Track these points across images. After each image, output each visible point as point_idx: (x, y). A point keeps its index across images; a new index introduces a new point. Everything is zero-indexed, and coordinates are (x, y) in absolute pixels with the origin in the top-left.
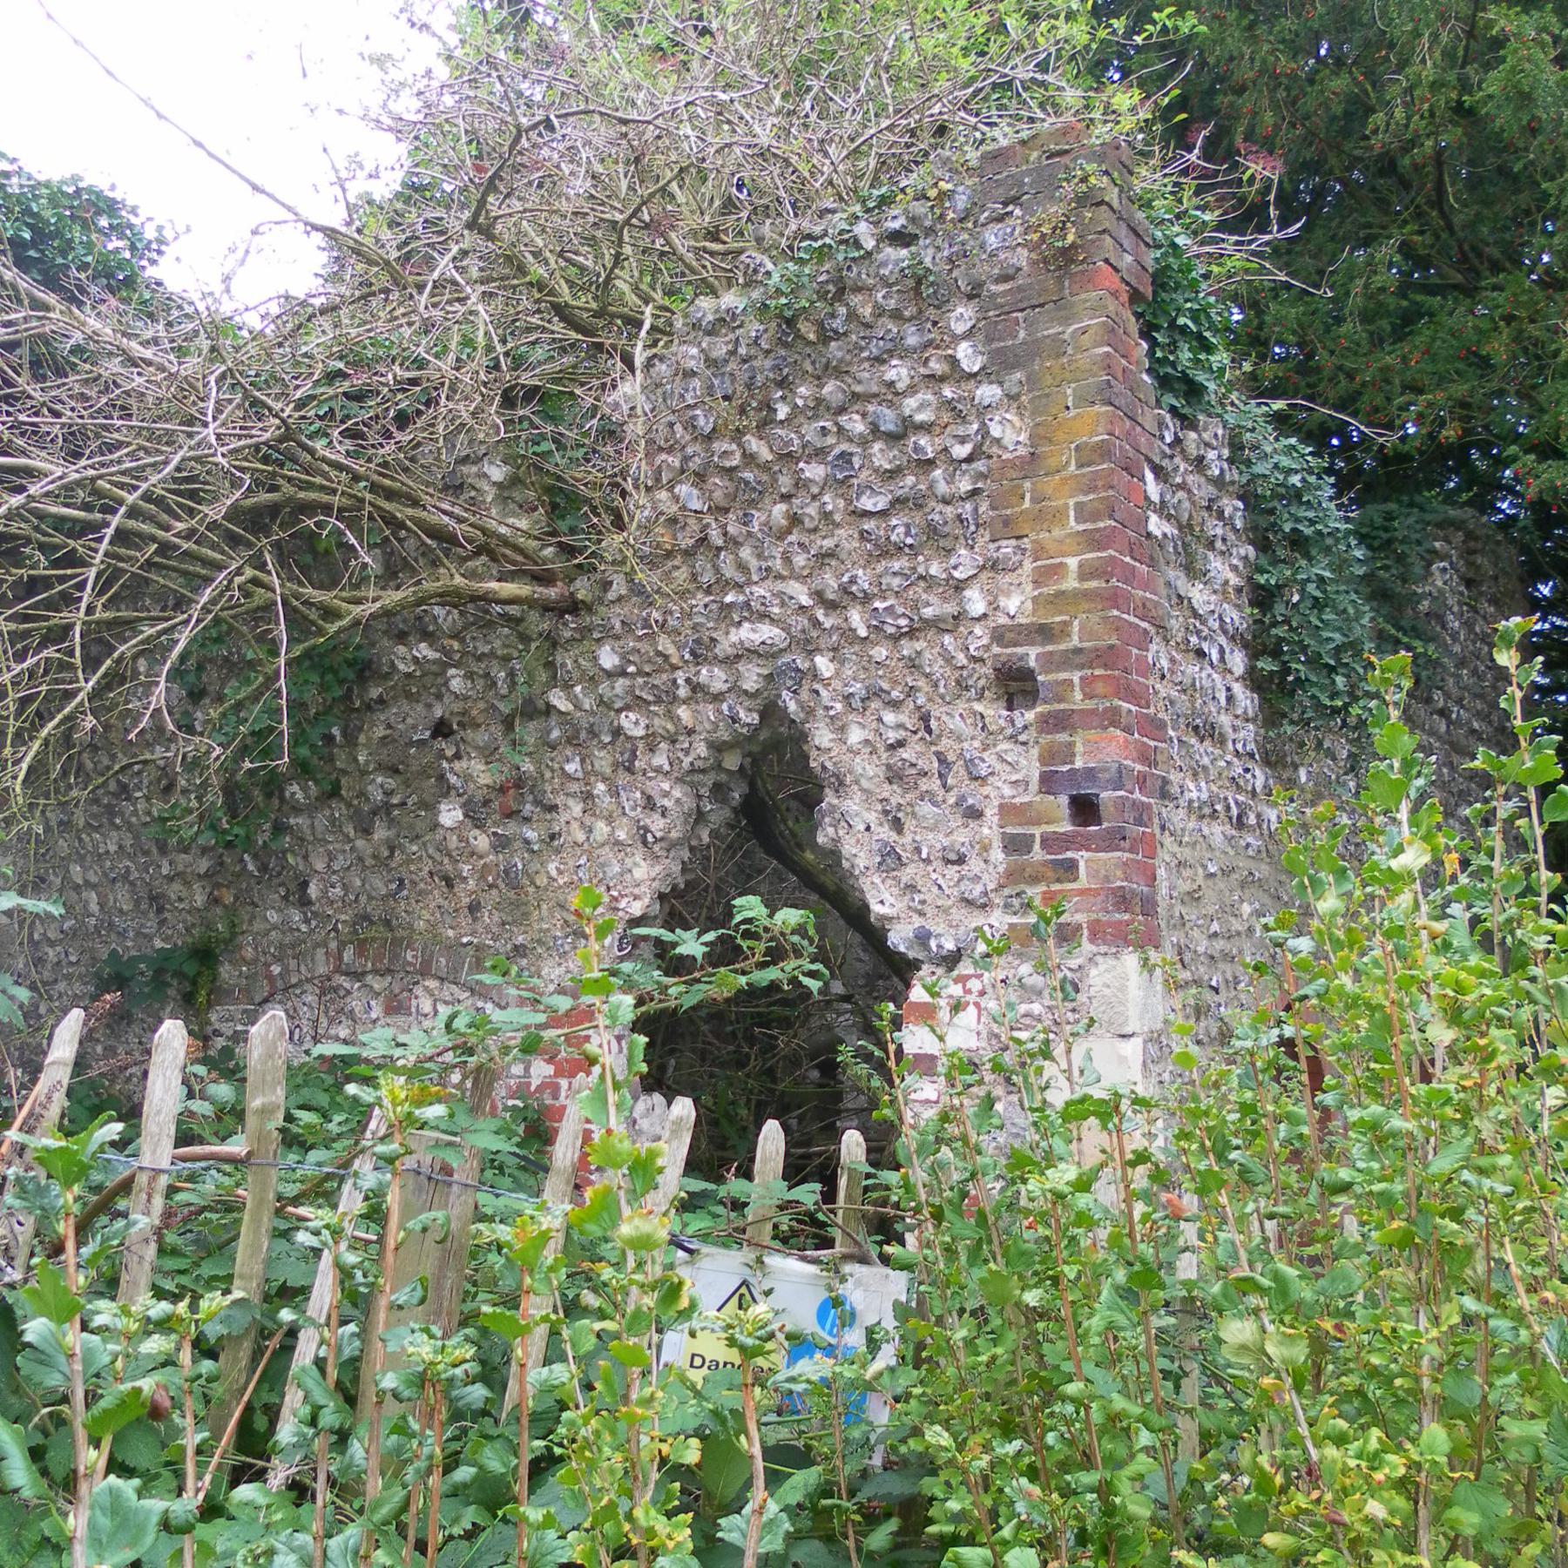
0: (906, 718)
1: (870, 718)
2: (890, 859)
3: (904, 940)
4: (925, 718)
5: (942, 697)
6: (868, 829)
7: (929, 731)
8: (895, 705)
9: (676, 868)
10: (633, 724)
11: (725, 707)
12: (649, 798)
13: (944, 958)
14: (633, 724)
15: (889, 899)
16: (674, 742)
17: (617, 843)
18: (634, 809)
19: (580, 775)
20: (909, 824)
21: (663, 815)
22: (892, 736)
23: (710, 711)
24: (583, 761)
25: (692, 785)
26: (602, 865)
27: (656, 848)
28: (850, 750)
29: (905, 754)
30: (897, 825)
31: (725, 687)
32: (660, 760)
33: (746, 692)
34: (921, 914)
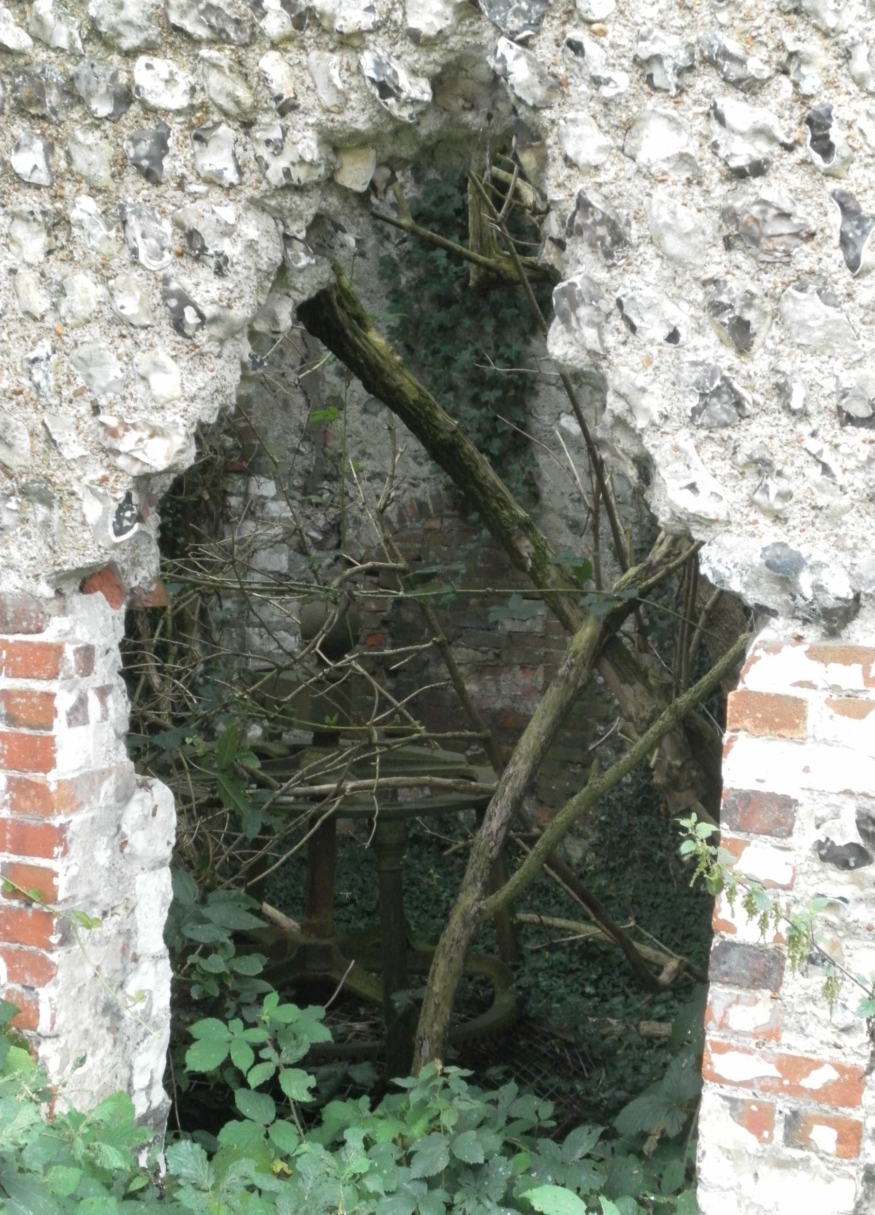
0: (774, 112)
1: (691, 111)
2: (719, 403)
3: (743, 569)
4: (818, 125)
5: (860, 81)
6: (673, 337)
7: (826, 149)
8: (749, 87)
9: (233, 377)
10: (162, 81)
11: (367, 60)
12: (192, 235)
13: (827, 614)
14: (162, 81)
15: (706, 484)
16: (247, 125)
17: (118, 320)
18: (158, 254)
19: (42, 177)
20: (765, 334)
21: (219, 272)
22: (743, 153)
23: (330, 66)
24: (49, 150)
25: (280, 215)
26: (86, 362)
27: (202, 337)
28: (644, 173)
29: (771, 189)
30: (741, 335)
31: (367, 21)
32: (218, 159)
33: (414, 36)
34: (778, 518)
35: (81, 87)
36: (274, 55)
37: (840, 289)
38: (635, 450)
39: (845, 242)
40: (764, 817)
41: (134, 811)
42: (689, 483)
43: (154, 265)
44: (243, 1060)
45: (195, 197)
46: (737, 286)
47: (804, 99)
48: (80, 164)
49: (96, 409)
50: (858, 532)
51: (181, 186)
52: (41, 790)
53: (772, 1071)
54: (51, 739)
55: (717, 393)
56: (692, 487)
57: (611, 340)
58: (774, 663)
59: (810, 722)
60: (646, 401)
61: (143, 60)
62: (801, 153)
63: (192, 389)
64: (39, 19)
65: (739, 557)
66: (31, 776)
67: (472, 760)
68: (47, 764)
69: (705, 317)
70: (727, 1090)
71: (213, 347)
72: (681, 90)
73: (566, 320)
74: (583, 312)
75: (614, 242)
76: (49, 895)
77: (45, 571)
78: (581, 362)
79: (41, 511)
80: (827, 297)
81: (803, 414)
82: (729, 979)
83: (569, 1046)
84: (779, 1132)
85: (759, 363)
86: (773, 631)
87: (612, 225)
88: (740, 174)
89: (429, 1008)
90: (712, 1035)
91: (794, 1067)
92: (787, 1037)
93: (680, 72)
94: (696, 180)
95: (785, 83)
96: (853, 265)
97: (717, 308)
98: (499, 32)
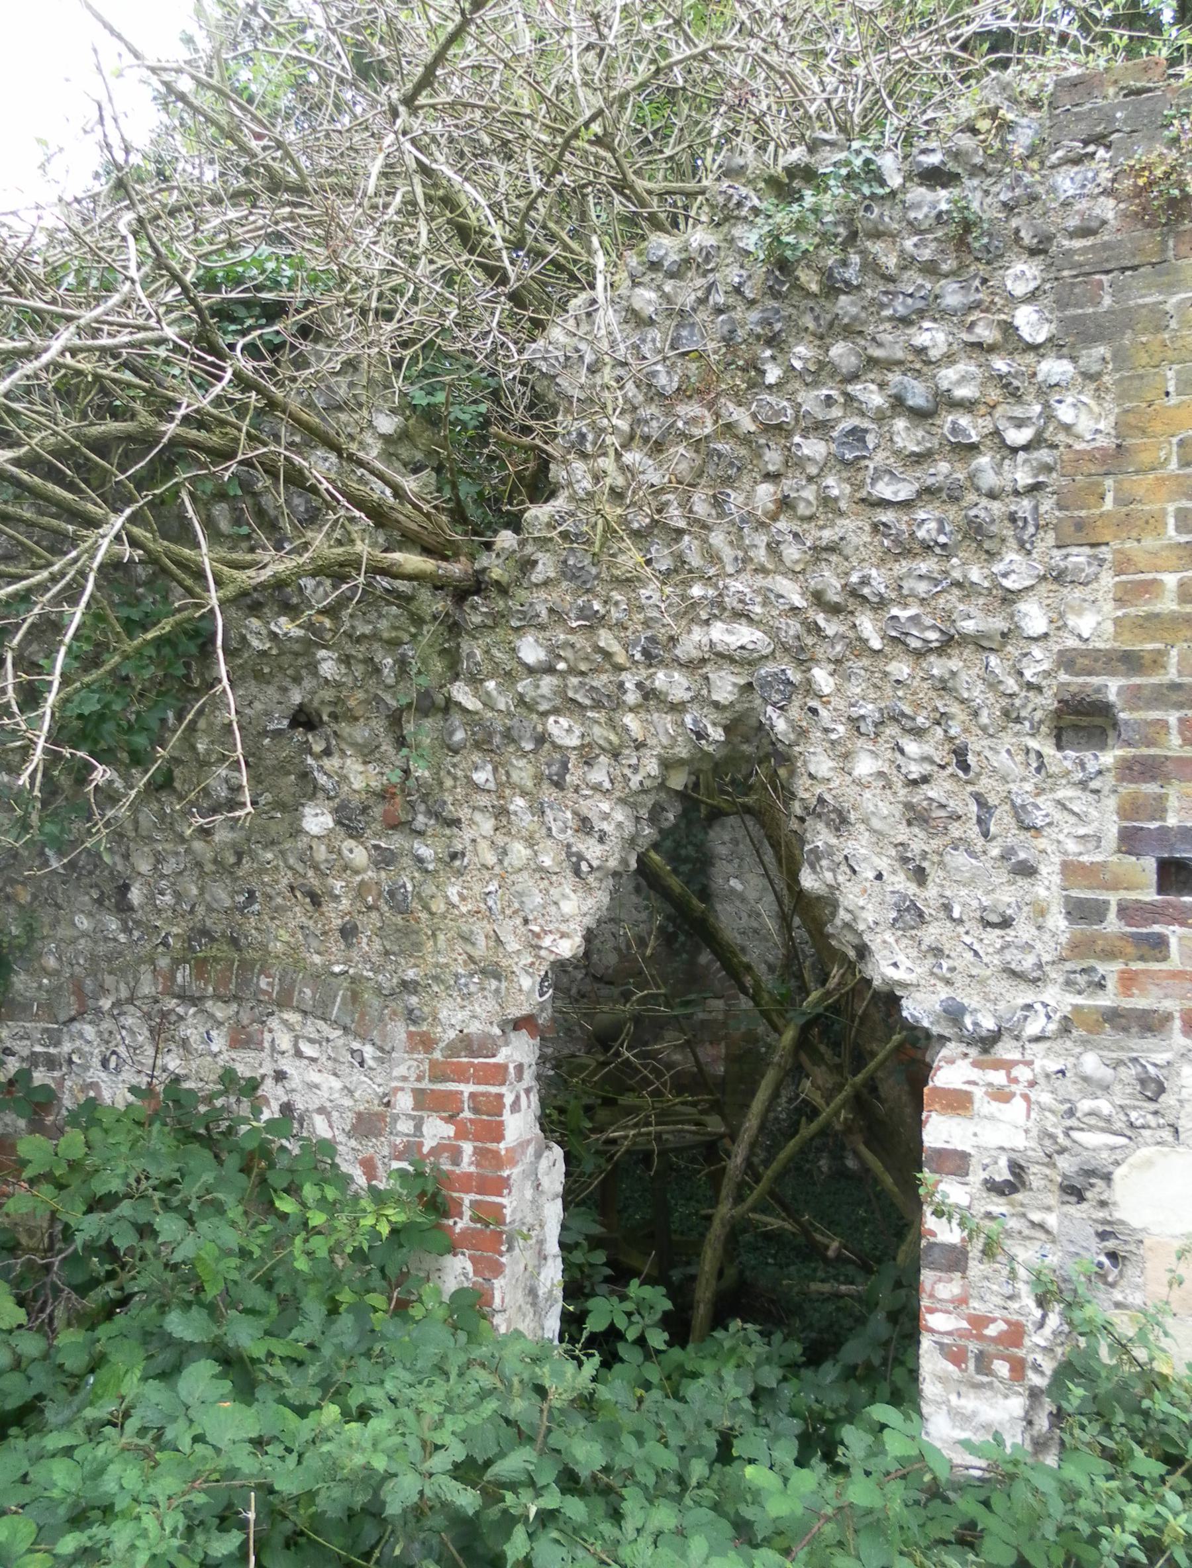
1: (883, 747)
2: (909, 916)
4: (960, 755)
5: (984, 729)
6: (879, 877)
7: (966, 768)
8: (918, 733)
9: (606, 900)
12: (585, 820)
13: (983, 1040)
17: (540, 869)
18: (563, 831)
19: (491, 786)
20: (935, 875)
21: (601, 840)
22: (915, 770)
23: (667, 722)
24: (495, 770)
25: (634, 806)
26: (520, 894)
27: (591, 879)
28: (857, 782)
30: (920, 876)
31: (687, 696)
32: (598, 775)
33: (716, 705)
34: (948, 982)
35: (515, 733)
36: (631, 716)
37: (978, 849)
38: (856, 941)
39: (980, 821)
40: (950, 1165)
41: (544, 1164)
42: (891, 962)
43: (561, 837)
44: (621, 1323)
45: (586, 797)
46: (916, 847)
47: (951, 739)
48: (515, 776)
49: (526, 921)
50: (997, 990)
51: (576, 791)
52: (496, 1154)
53: (965, 1324)
54: (501, 1123)
55: (908, 909)
56: (895, 965)
57: (841, 879)
58: (951, 1071)
59: (976, 1105)
60: (864, 914)
61: (552, 719)
62: (950, 770)
63: (585, 909)
64: (488, 694)
65: (927, 1006)
66: (489, 1145)
67: (702, 1112)
68: (500, 1138)
69: (897, 865)
70: (936, 1337)
71: (595, 884)
72: (877, 735)
73: (813, 867)
74: (824, 863)
75: (840, 821)
76: (501, 1221)
77: (496, 1020)
78: (822, 890)
79: (494, 983)
80: (972, 854)
81: (960, 921)
82: (934, 1267)
83: (772, 1301)
84: (971, 1365)
85: (932, 891)
86: (951, 1049)
87: (840, 813)
88: (914, 783)
89: (702, 1281)
90: (925, 1302)
91: (978, 1322)
92: (974, 1303)
93: (876, 725)
94: (888, 785)
95: (939, 731)
96: (985, 834)
97: (905, 860)
98: (766, 701)
